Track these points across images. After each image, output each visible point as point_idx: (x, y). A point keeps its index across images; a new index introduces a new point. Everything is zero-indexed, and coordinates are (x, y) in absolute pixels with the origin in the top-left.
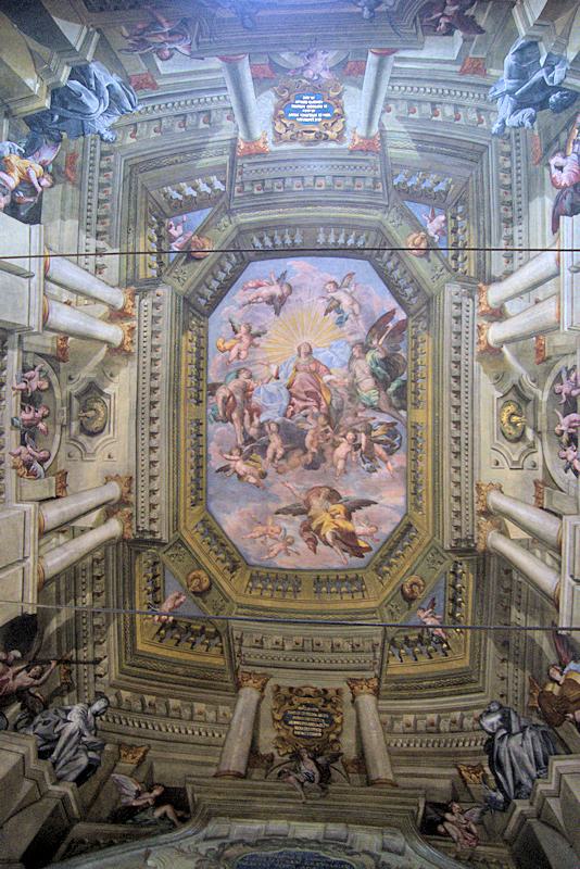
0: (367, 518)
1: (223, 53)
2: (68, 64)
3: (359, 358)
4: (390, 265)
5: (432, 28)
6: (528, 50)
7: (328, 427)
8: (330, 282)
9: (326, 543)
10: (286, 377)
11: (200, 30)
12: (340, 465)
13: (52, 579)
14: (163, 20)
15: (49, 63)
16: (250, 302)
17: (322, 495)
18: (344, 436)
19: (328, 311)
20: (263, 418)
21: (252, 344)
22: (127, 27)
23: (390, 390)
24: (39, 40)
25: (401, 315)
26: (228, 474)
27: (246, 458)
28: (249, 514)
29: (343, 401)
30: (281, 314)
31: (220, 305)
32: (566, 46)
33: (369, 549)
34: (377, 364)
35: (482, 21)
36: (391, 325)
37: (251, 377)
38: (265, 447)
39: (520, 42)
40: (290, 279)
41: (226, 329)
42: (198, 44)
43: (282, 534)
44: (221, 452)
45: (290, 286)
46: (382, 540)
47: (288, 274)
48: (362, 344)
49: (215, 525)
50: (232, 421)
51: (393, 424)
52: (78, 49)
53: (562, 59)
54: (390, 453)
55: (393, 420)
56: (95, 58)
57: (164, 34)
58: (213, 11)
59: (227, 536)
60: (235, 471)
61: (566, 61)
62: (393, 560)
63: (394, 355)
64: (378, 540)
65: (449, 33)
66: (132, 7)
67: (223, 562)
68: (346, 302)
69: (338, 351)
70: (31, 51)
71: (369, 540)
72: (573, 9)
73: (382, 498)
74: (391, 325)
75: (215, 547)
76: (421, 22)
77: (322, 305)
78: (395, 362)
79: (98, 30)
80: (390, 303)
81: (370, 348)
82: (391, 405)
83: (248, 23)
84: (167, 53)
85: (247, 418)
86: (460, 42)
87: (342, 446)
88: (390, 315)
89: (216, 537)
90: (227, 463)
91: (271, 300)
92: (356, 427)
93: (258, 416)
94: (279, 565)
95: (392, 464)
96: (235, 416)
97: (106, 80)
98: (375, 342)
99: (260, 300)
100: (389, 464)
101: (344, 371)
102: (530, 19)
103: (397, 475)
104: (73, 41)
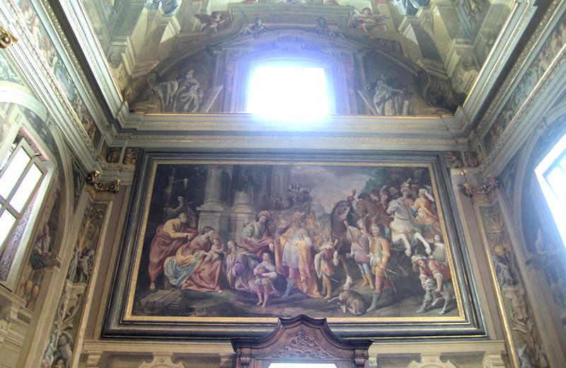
1: (337, 7)
2: (417, 18)
5: (224, 15)
6: (170, 9)
11: (347, 22)
14: (365, 29)
15: (426, 22)
22: (383, 29)
24: (427, 34)
32: (148, 15)
35: (197, 21)
39: (174, 12)
42: (349, 14)
52: (410, 25)
53: (150, 8)
56: (403, 17)
57: (366, 22)
58: (340, 30)
61: (148, 7)
65: (214, 14)
66: (379, 39)
70: (433, 30)
76: (230, 19)
79: (398, 32)
83: (322, 21)
84: (365, 12)
86: (208, 9)
97: (399, 4)
102: (171, 25)
104: (412, 30)
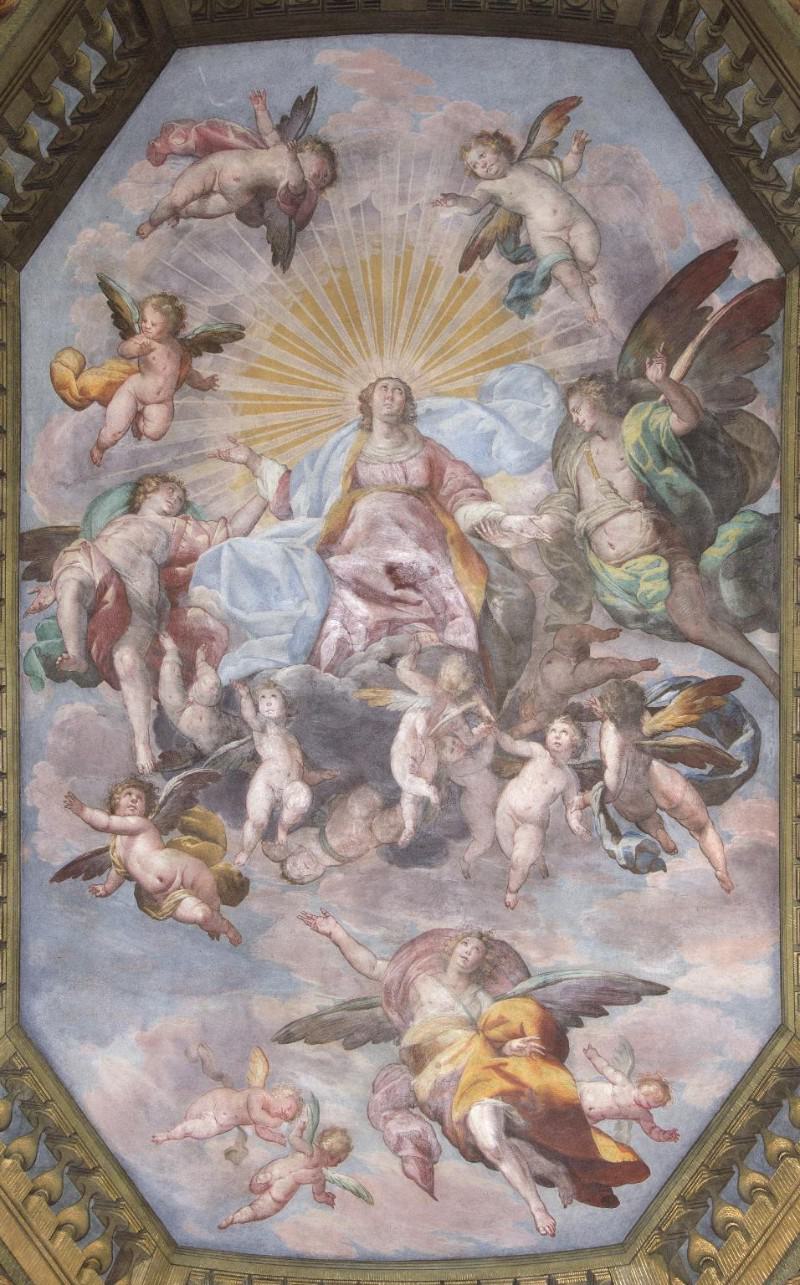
0: (626, 1047)
3: (595, 432)
4: (717, 65)
7: (477, 702)
8: (483, 137)
9: (472, 1152)
10: (315, 512)
12: (523, 847)
13: (481, 483)
16: (175, 213)
17: (456, 962)
18: (539, 736)
19: (473, 253)
20: (232, 669)
21: (186, 379)
23: (715, 555)
25: (757, 265)
26: (102, 883)
27: (169, 822)
28: (177, 1040)
29: (530, 604)
30: (295, 265)
31: (63, 224)
33: (636, 1170)
34: (664, 458)
36: (718, 301)
37: (184, 508)
38: (240, 780)
40: (327, 122)
41: (89, 322)
43: (305, 1118)
44: (73, 803)
45: (327, 151)
46: (687, 1134)
47: (323, 105)
48: (606, 377)
49: (48, 1089)
50: (115, 683)
51: (728, 684)
54: (715, 793)
55: (726, 669)
59: (94, 1131)
60: (128, 876)
62: (731, 1212)
63: (731, 416)
64: (672, 1135)
67: (79, 1237)
68: (543, 214)
69: (513, 407)
71: (636, 1137)
72: (321, 994)
73: (684, 969)
74: (718, 301)
75: (51, 1179)
77: (452, 226)
78: (733, 445)
80: (726, 219)
81: (633, 399)
82: (716, 615)
85: (169, 670)
87: (529, 772)
88: (715, 263)
89: (54, 1137)
90: (98, 842)
91: (256, 203)
92: (582, 699)
93: (214, 662)
94: (293, 1244)
95: (724, 838)
96: (125, 658)
98: (654, 372)
99: (216, 202)
100: (711, 836)
101: (535, 486)
103: (741, 879)
